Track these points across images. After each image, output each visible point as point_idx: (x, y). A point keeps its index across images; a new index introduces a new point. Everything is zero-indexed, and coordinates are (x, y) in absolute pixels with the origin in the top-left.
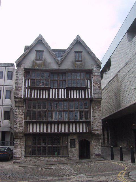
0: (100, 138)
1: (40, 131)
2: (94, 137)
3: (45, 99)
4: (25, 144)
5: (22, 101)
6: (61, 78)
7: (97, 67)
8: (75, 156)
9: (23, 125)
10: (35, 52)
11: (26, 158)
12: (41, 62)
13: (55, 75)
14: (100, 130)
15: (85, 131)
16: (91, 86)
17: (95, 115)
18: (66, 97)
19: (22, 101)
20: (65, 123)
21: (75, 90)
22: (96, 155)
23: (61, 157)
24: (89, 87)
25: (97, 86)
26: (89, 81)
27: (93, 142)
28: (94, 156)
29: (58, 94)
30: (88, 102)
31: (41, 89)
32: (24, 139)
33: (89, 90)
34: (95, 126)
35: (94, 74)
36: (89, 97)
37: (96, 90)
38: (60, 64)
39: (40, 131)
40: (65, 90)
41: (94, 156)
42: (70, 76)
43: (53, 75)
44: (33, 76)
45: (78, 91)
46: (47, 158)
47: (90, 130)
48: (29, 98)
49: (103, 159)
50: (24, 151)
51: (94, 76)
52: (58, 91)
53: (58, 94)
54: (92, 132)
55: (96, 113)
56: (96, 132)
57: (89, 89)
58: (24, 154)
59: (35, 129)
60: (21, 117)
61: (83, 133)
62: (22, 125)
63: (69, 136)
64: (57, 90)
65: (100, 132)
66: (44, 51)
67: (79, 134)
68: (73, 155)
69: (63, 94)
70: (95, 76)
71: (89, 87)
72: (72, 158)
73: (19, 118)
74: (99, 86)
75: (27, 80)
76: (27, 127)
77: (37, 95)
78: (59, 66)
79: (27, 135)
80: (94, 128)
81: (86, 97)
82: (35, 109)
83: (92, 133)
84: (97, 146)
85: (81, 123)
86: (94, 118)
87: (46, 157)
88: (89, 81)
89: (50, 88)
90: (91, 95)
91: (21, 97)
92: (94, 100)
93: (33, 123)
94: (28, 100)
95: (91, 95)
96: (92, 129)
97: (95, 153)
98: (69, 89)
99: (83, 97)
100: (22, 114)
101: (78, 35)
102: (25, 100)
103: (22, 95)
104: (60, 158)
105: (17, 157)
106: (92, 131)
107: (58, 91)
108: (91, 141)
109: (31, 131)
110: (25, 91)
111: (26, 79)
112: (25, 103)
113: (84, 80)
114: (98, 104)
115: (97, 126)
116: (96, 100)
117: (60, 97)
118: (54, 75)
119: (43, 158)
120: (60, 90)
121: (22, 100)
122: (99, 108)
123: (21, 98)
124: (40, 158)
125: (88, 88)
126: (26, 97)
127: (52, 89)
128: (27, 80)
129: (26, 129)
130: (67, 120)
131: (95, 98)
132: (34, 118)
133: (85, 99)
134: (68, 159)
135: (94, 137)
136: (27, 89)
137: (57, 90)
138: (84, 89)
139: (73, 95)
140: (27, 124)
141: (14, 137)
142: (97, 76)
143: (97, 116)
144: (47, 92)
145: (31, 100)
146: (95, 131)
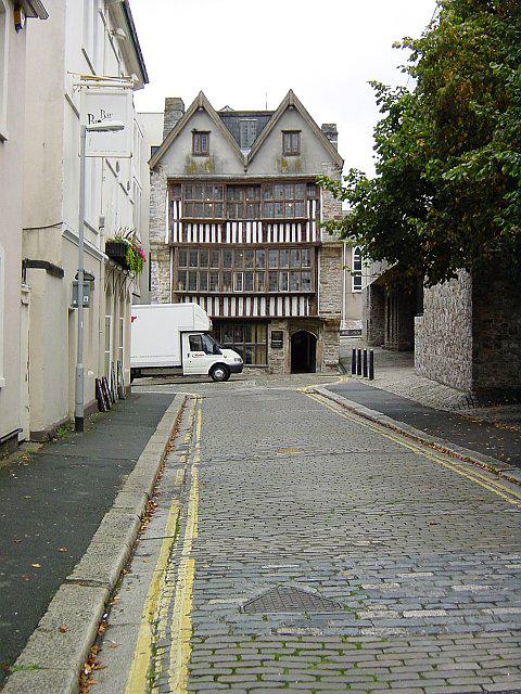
3: (217, 247)
24: (314, 217)
52: (244, 228)
61: (298, 318)
71: (314, 217)
102: (172, 247)
107: (244, 228)
110: (172, 229)
117: (248, 241)
120: (248, 224)
125: (311, 220)
132: (203, 285)
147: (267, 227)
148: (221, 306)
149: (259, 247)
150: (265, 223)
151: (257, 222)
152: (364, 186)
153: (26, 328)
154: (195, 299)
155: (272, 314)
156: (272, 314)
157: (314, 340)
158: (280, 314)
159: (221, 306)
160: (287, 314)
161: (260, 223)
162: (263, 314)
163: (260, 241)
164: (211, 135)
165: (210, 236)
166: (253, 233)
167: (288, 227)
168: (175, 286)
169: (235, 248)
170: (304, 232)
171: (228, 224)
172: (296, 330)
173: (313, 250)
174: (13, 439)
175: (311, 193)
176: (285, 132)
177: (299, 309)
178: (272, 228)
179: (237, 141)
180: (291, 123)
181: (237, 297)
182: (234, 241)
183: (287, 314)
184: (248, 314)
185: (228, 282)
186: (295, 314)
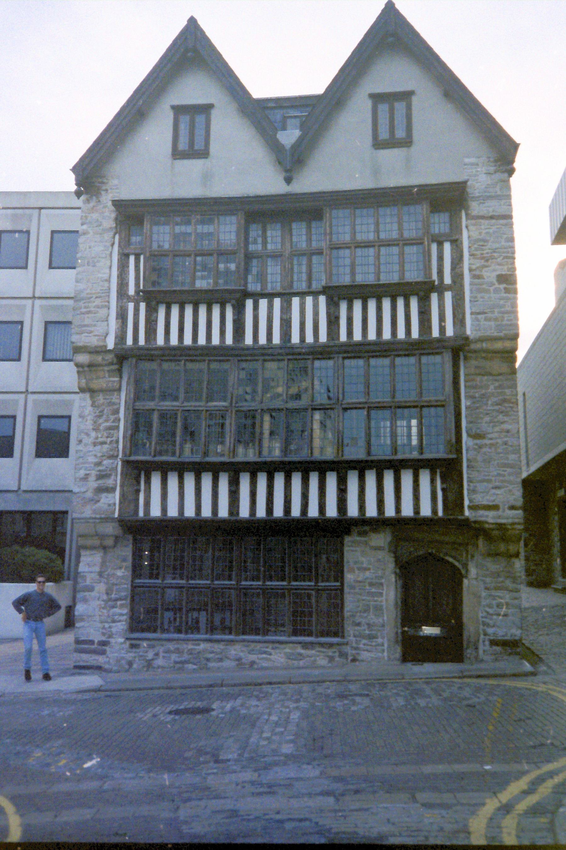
0: (512, 548)
1: (164, 509)
2: (481, 542)
4: (129, 573)
5: (112, 364)
6: (299, 233)
7: (492, 169)
8: (380, 640)
9: (117, 480)
11: (133, 646)
13: (268, 226)
14: (512, 508)
15: (426, 511)
16: (458, 277)
17: (484, 425)
18: (415, 334)
19: (112, 364)
20: (322, 467)
22: (494, 643)
23: (306, 646)
24: (448, 280)
25: (490, 275)
26: (447, 246)
27: (473, 571)
28: (484, 647)
29: (286, 324)
30: (441, 363)
31: (197, 298)
33: (448, 296)
34: (480, 487)
35: (476, 208)
36: (450, 332)
37: (486, 296)
38: (292, 161)
39: (398, 509)
40: (322, 299)
41: (484, 647)
42: (342, 225)
43: (260, 226)
44: (162, 236)
45: (400, 303)
46: (238, 647)
47: (454, 501)
48: (141, 348)
49: (527, 666)
50: (125, 611)
52: (286, 309)
53: (286, 324)
54: (467, 519)
55: (487, 419)
56: (489, 517)
57: (449, 288)
58: (121, 626)
59: (173, 499)
60: (109, 440)
61: (417, 522)
62: (110, 482)
63: (347, 539)
65: (512, 517)
66: (211, 106)
67: (401, 529)
68: (371, 637)
69: (309, 320)
70: (483, 217)
71: (448, 280)
72: (365, 655)
74: (503, 270)
75: (132, 259)
76: (138, 491)
77: (180, 328)
78: (288, 180)
79: (146, 535)
80: (481, 499)
81: (431, 333)
82: (171, 404)
83: (466, 524)
84: (499, 593)
86: (478, 442)
87: (311, 645)
89: (246, 294)
90: (459, 321)
91: (106, 346)
92: (473, 346)
93: (165, 469)
95: (459, 321)
96: (466, 503)
97: (490, 631)
98: (336, 295)
99: (415, 334)
100: (110, 428)
101: (192, 21)
102: (121, 357)
103: (105, 331)
104: (300, 650)
105: (92, 642)
106: (467, 513)
107: (286, 309)
108: (465, 566)
109: (156, 512)
110: (122, 316)
111: (127, 256)
113: (417, 242)
114: (497, 366)
115: (496, 488)
116: (484, 345)
117: (295, 339)
118: (309, 228)
119: (218, 647)
120: (296, 301)
122: (508, 391)
123: (101, 350)
124: (202, 646)
125: (440, 289)
126: (129, 341)
127: (256, 297)
128: (132, 259)
129: (129, 499)
130: (329, 454)
131: (481, 340)
133: (422, 347)
134: (343, 655)
135: (481, 542)
136: (131, 306)
137: (277, 302)
138: (424, 290)
139: (364, 323)
140: (138, 471)
142: (492, 217)
143: (496, 435)
145: (151, 358)
146: (486, 513)
147: (337, 306)
149: (320, 352)
152: (283, 226)
153: (414, 430)
155: (353, 511)
156: (353, 511)
157: (456, 578)
158: (371, 511)
160: (390, 512)
162: (332, 512)
164: (214, 113)
165: (209, 328)
168: (134, 443)
170: (425, 314)
171: (249, 303)
172: (409, 550)
173: (448, 357)
174: (3, 695)
175: (440, 224)
177: (418, 497)
178: (350, 309)
180: (193, 89)
182: (262, 340)
183: (390, 512)
184: (296, 512)
186: (407, 511)
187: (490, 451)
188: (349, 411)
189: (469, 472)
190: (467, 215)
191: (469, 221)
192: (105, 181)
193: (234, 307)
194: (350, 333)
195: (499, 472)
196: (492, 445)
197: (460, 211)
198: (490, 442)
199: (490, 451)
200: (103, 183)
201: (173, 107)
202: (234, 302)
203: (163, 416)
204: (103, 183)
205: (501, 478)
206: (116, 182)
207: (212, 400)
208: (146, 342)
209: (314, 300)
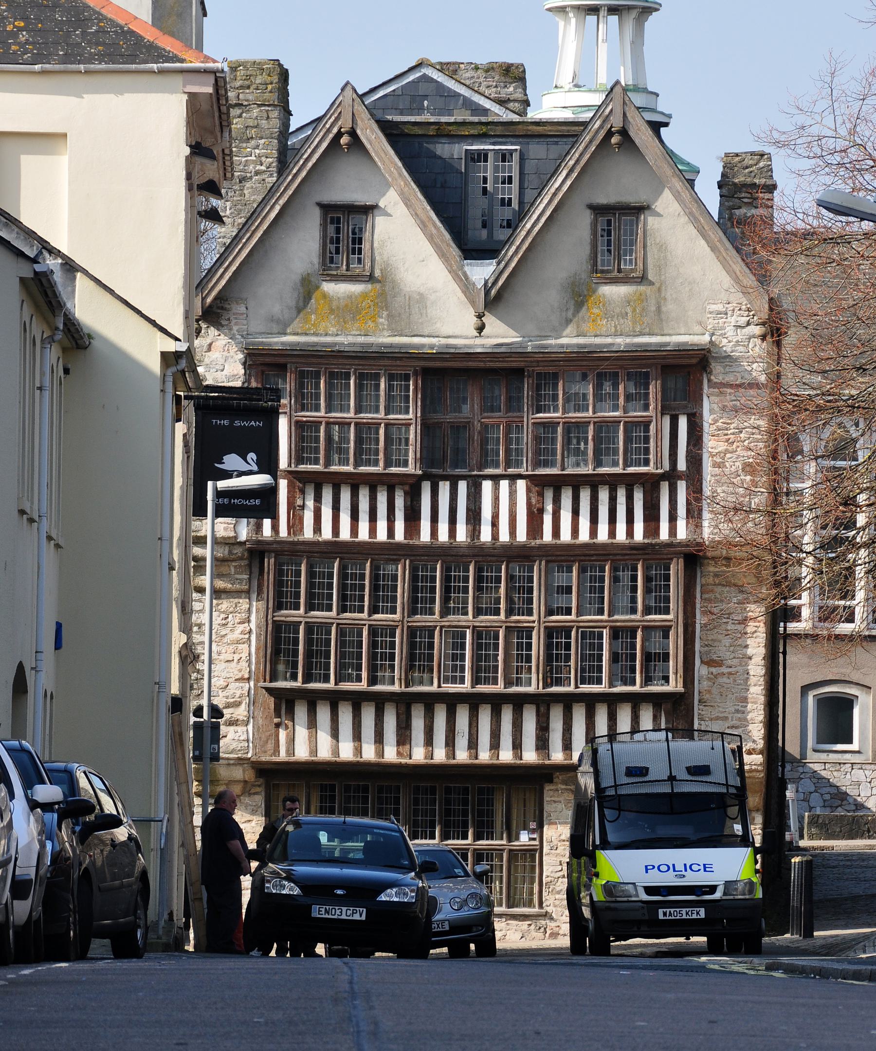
3: (391, 552)
5: (241, 558)
10: (317, 213)
12: (356, 288)
19: (241, 558)
21: (585, 483)
24: (682, 466)
32: (259, 800)
51: (723, 385)
55: (727, 641)
60: (237, 657)
63: (548, 787)
64: (462, 486)
71: (682, 466)
73: (224, 665)
85: (578, 702)
88: (683, 422)
91: (236, 537)
94: (278, 554)
112: (256, 570)
120: (487, 486)
121: (238, 551)
125: (672, 476)
132: (590, 674)
137: (462, 486)
141: (220, 110)
144: (400, 502)
147: (541, 495)
148: (543, 730)
150: (538, 484)
151: (513, 478)
154: (323, 714)
159: (543, 730)
161: (521, 484)
163: (522, 536)
166: (504, 510)
167: (604, 495)
169: (451, 556)
173: (676, 569)
176: (598, 210)
179: (468, 228)
181: (452, 701)
185: (419, 658)
187: (728, 681)
188: (667, 113)
189: (701, 707)
190: (709, 380)
191: (711, 390)
192: (227, 306)
193: (406, 494)
194: (556, 533)
195: (737, 707)
196: (730, 673)
197: (702, 375)
198: (730, 670)
199: (728, 681)
200: (222, 308)
201: (321, 206)
202: (407, 488)
203: (310, 628)
204: (222, 308)
205: (739, 715)
206: (242, 309)
207: (447, 838)
208: (289, 533)
209: (510, 486)
